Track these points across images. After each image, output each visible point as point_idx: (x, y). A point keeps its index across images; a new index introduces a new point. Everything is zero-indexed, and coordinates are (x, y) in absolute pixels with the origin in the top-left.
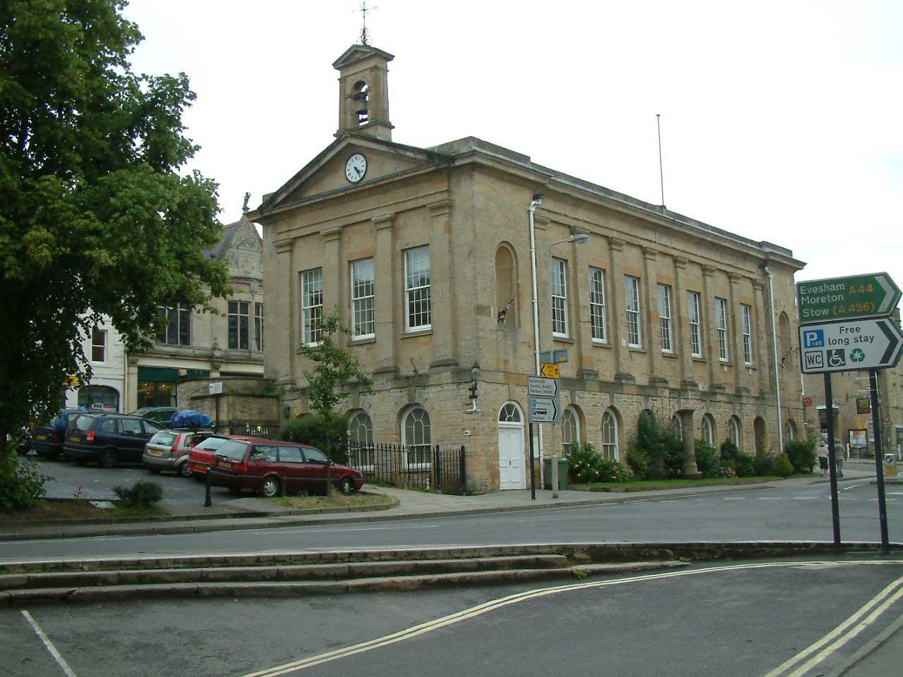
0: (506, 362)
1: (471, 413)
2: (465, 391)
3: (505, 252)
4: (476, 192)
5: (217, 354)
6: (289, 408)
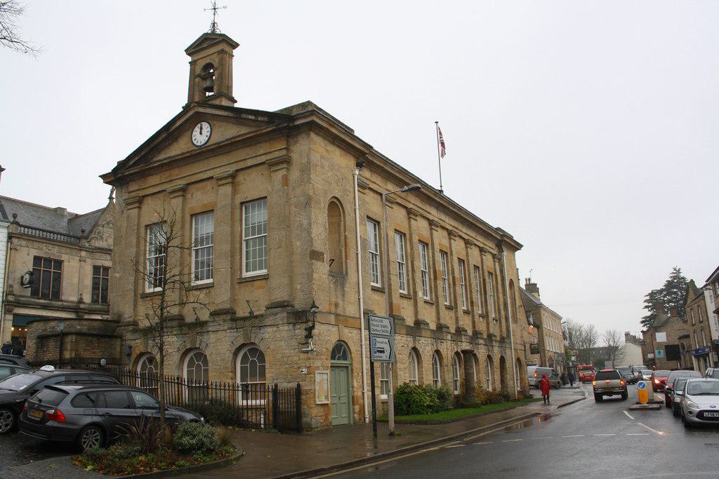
0: (336, 305)
1: (307, 352)
2: (300, 332)
3: (335, 206)
4: (314, 148)
5: (82, 306)
6: (130, 347)
